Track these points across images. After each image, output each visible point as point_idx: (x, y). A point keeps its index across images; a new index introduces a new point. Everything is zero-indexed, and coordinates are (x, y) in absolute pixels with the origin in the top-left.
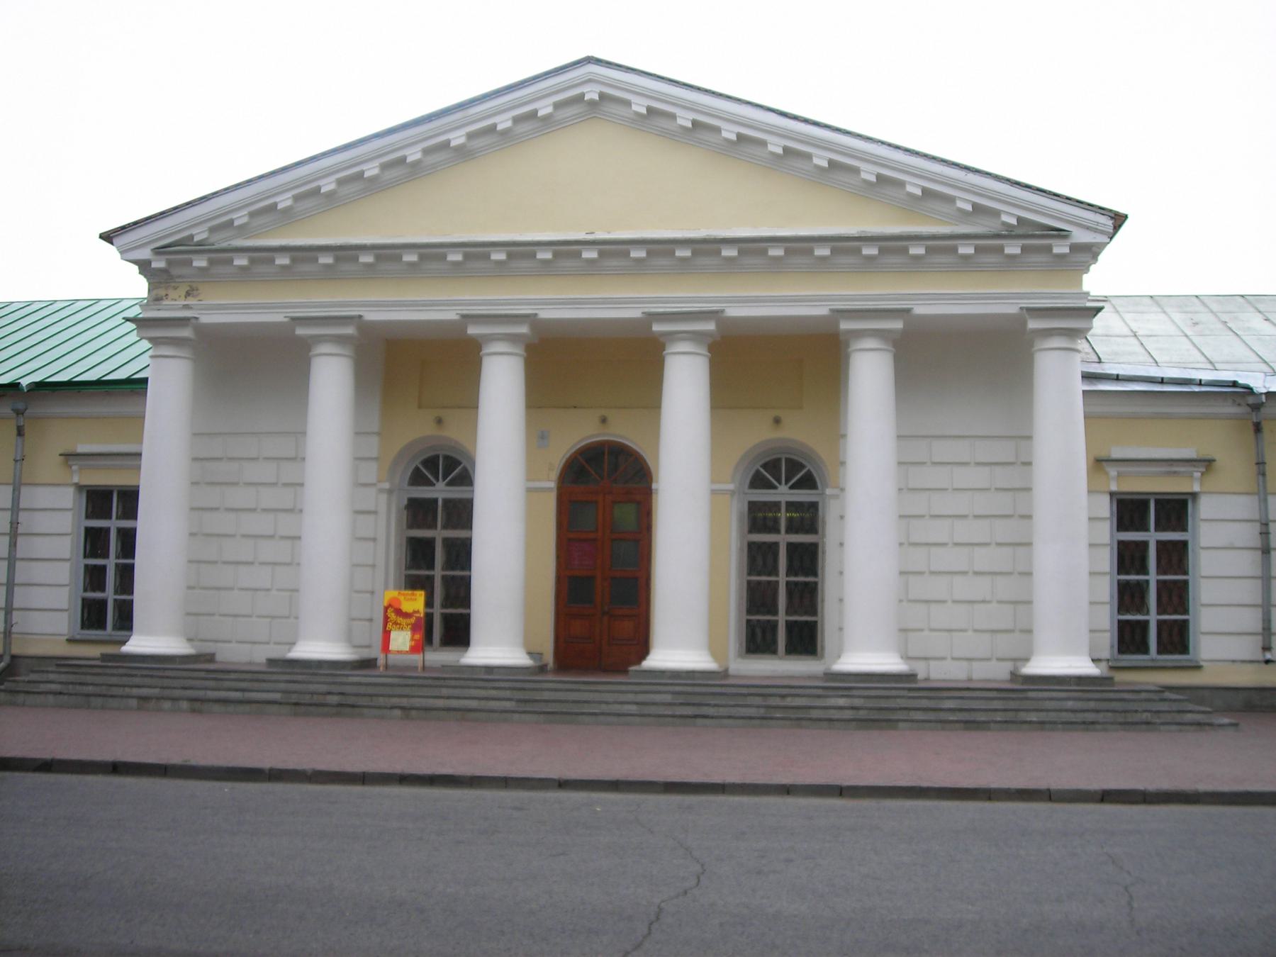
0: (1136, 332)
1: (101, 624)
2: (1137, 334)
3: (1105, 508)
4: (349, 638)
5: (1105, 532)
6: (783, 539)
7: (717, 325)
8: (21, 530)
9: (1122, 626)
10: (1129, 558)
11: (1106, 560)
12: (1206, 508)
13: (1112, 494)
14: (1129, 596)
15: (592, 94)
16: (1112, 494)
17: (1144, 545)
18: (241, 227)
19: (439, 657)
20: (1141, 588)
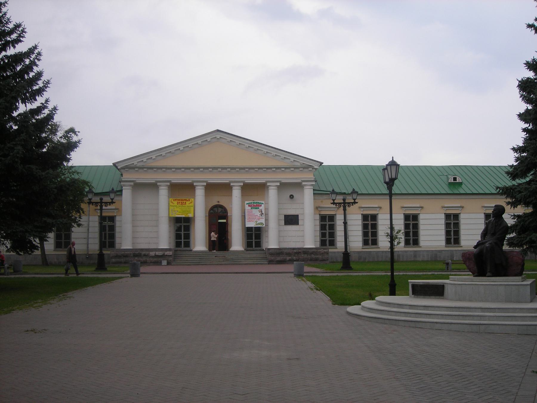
0: (113, 189)
1: (326, 245)
2: (115, 190)
3: (318, 217)
4: (315, 246)
5: (318, 223)
6: (328, 223)
7: (170, 184)
8: (90, 226)
9: (177, 242)
10: (323, 227)
11: (318, 228)
12: (380, 217)
13: (362, 214)
14: (323, 235)
15: (218, 137)
16: (362, 214)
17: (326, 225)
18: (154, 159)
19: (371, 249)
20: (325, 233)
